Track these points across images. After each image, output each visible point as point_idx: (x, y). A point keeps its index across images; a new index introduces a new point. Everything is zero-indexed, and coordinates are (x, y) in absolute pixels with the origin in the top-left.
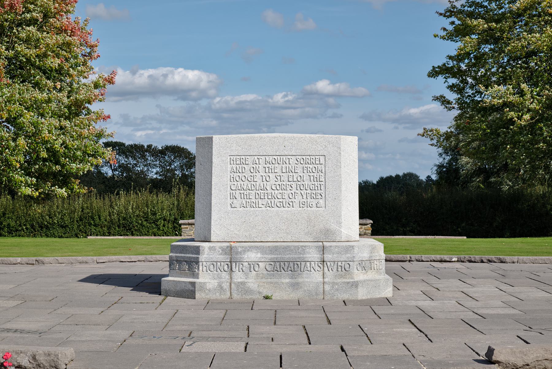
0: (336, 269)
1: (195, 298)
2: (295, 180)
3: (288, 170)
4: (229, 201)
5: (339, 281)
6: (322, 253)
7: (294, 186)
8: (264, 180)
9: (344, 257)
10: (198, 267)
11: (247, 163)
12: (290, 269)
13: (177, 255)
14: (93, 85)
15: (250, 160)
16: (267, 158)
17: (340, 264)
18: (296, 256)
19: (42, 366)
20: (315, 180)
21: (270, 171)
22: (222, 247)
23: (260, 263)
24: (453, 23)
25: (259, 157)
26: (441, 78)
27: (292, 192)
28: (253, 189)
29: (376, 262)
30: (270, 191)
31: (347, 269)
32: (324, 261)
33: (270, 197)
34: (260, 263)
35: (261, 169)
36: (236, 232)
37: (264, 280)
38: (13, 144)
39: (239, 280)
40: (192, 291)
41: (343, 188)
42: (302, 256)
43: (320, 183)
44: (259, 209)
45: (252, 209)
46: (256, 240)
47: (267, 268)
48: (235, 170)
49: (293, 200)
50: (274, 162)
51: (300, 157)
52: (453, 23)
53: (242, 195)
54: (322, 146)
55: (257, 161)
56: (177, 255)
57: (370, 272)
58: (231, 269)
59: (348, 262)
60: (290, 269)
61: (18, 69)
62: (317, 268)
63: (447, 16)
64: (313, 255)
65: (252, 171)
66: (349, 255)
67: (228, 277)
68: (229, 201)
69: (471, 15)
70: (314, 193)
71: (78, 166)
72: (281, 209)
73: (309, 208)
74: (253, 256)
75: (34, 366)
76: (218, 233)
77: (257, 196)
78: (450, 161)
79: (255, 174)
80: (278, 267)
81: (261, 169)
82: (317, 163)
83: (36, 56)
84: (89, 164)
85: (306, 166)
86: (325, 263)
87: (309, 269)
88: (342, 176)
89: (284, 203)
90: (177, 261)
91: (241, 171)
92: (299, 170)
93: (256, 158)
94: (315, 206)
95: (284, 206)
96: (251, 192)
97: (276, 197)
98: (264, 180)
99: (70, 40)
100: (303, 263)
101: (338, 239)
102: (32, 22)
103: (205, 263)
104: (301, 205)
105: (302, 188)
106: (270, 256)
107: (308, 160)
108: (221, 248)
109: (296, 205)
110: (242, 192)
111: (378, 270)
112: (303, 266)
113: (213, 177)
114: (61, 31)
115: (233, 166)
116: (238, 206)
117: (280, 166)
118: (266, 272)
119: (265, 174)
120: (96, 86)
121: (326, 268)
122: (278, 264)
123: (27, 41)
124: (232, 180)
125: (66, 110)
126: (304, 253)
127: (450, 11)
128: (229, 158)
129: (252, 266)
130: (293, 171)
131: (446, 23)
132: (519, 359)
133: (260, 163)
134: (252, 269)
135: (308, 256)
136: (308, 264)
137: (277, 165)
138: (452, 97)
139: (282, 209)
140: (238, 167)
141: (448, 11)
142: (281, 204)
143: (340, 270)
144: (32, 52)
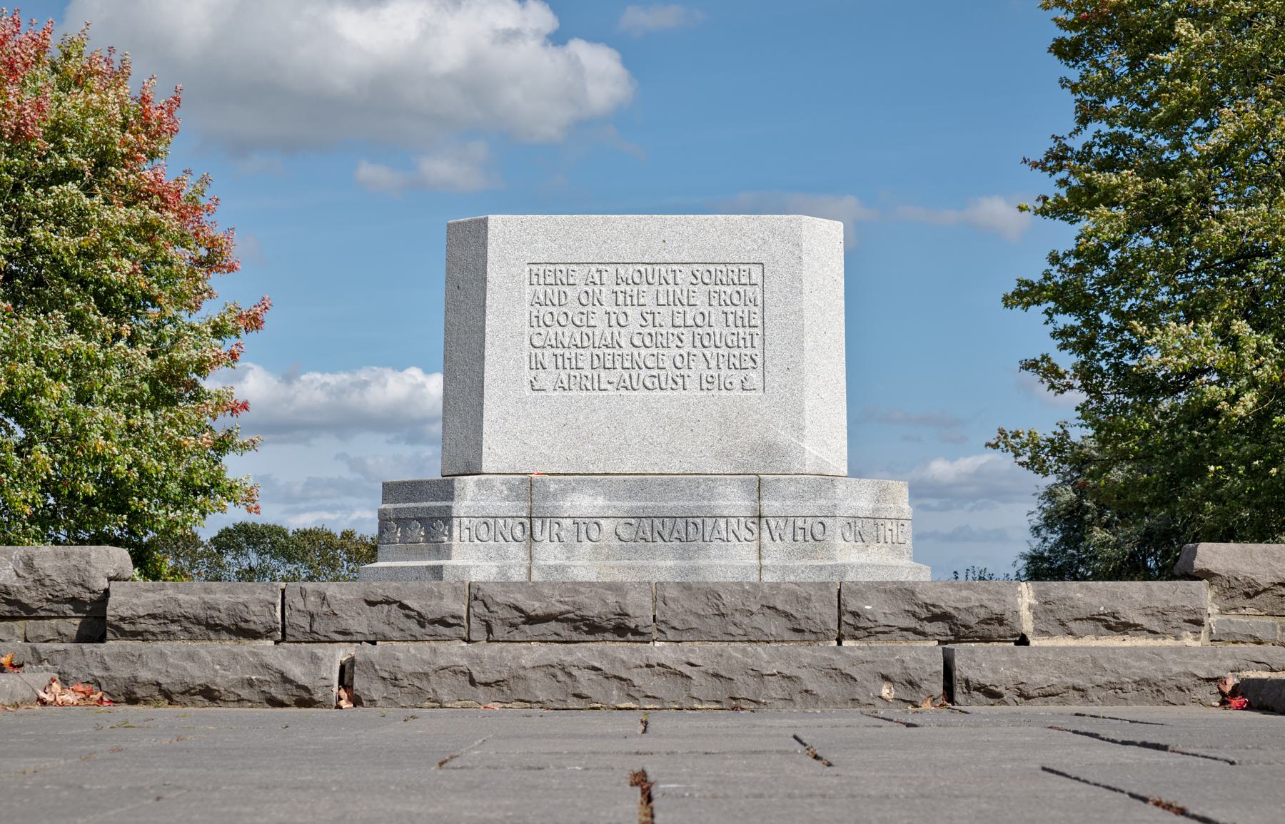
0: (790, 536)
2: (689, 322)
3: (671, 298)
4: (528, 375)
5: (797, 563)
6: (755, 496)
7: (687, 338)
8: (613, 322)
9: (810, 507)
10: (450, 531)
11: (571, 281)
12: (676, 535)
13: (398, 505)
14: (209, 330)
15: (579, 274)
17: (800, 523)
18: (691, 504)
19: (47, 582)
20: (739, 323)
21: (629, 302)
22: (509, 482)
23: (602, 521)
24: (1064, 182)
25: (600, 267)
26: (1037, 311)
27: (681, 351)
28: (585, 344)
29: (889, 525)
30: (627, 349)
31: (819, 537)
32: (760, 517)
33: (627, 364)
34: (602, 521)
35: (606, 297)
36: (544, 450)
37: (613, 563)
38: (17, 461)
39: (552, 562)
41: (808, 343)
42: (706, 503)
43: (752, 330)
44: (601, 393)
45: (584, 393)
46: (592, 469)
47: (620, 531)
48: (542, 298)
49: (685, 372)
50: (637, 280)
51: (701, 268)
52: (1064, 182)
53: (560, 359)
54: (755, 241)
55: (597, 276)
56: (398, 505)
57: (874, 547)
58: (531, 535)
59: (820, 519)
60: (676, 535)
61: (30, 284)
62: (744, 533)
63: (1050, 168)
64: (734, 501)
65: (584, 302)
66: (822, 502)
67: (523, 554)
68: (528, 375)
69: (1108, 165)
70: (737, 354)
71: (171, 515)
72: (654, 393)
73: (724, 392)
74: (584, 502)
75: (29, 583)
76: (498, 451)
77: (596, 361)
78: (1057, 545)
79: (590, 308)
80: (648, 529)
81: (606, 297)
82: (743, 281)
83: (78, 254)
84: (197, 511)
85: (717, 288)
86: (763, 521)
87: (724, 535)
88: (806, 313)
89: (663, 379)
90: (398, 520)
91: (556, 302)
93: (594, 268)
94: (739, 386)
95: (663, 386)
96: (581, 351)
97: (642, 365)
98: (613, 322)
99: (156, 219)
100: (709, 522)
101: (796, 467)
102: (71, 174)
103: (466, 521)
104: (705, 385)
105: (706, 344)
106: (627, 504)
107: (721, 275)
110: (558, 352)
111: (896, 544)
112: (709, 529)
113: (489, 317)
114: (136, 197)
115: (538, 288)
116: (549, 386)
117: (653, 288)
118: (616, 543)
119: (615, 309)
120: (218, 331)
121: (766, 534)
122: (646, 522)
123: (59, 217)
124: (535, 324)
125: (146, 386)
126: (712, 497)
127: (1056, 157)
128: (527, 269)
129: (583, 528)
130: (685, 301)
131: (1049, 186)
132: (1261, 569)
133: (604, 281)
134: (583, 536)
135: (720, 502)
136: (722, 522)
137: (645, 287)
138: (1067, 361)
139: (658, 393)
140: (549, 291)
141: (1051, 155)
142: (656, 381)
143: (800, 537)
144: (64, 243)
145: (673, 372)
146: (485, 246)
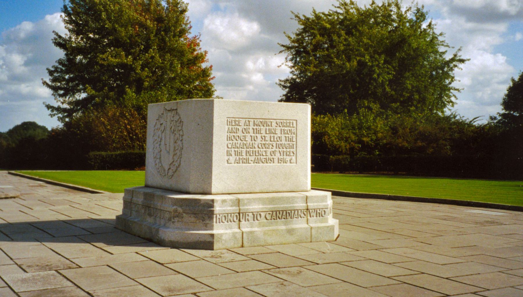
1: (213, 249)
4: (226, 158)
15: (242, 122)
16: (256, 120)
17: (318, 211)
30: (257, 149)
34: (262, 213)
40: (209, 242)
45: (244, 164)
47: (267, 216)
49: (274, 157)
51: (279, 121)
62: (302, 215)
68: (226, 158)
81: (251, 131)
92: (278, 132)
93: (247, 120)
103: (218, 215)
108: (231, 200)
109: (276, 161)
110: (236, 150)
112: (293, 214)
116: (233, 162)
117: (265, 127)
129: (255, 216)
137: (262, 127)
139: (266, 164)
145: (270, 157)
146: (212, 110)
